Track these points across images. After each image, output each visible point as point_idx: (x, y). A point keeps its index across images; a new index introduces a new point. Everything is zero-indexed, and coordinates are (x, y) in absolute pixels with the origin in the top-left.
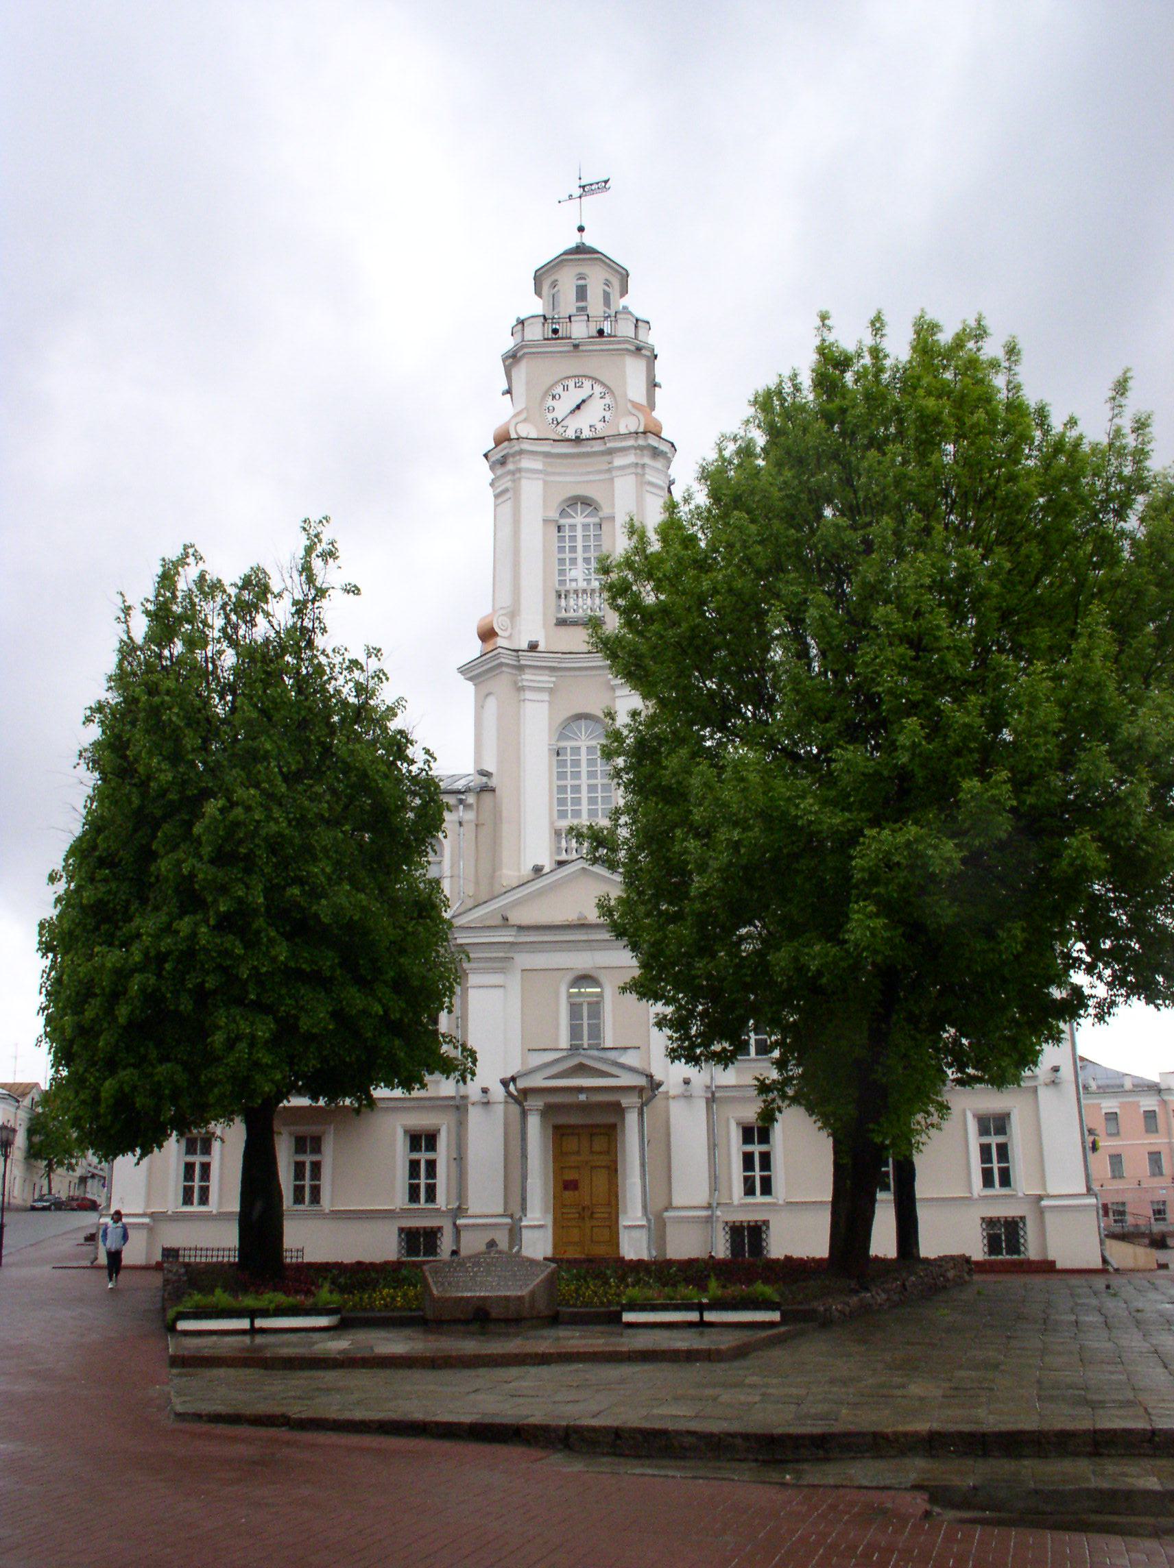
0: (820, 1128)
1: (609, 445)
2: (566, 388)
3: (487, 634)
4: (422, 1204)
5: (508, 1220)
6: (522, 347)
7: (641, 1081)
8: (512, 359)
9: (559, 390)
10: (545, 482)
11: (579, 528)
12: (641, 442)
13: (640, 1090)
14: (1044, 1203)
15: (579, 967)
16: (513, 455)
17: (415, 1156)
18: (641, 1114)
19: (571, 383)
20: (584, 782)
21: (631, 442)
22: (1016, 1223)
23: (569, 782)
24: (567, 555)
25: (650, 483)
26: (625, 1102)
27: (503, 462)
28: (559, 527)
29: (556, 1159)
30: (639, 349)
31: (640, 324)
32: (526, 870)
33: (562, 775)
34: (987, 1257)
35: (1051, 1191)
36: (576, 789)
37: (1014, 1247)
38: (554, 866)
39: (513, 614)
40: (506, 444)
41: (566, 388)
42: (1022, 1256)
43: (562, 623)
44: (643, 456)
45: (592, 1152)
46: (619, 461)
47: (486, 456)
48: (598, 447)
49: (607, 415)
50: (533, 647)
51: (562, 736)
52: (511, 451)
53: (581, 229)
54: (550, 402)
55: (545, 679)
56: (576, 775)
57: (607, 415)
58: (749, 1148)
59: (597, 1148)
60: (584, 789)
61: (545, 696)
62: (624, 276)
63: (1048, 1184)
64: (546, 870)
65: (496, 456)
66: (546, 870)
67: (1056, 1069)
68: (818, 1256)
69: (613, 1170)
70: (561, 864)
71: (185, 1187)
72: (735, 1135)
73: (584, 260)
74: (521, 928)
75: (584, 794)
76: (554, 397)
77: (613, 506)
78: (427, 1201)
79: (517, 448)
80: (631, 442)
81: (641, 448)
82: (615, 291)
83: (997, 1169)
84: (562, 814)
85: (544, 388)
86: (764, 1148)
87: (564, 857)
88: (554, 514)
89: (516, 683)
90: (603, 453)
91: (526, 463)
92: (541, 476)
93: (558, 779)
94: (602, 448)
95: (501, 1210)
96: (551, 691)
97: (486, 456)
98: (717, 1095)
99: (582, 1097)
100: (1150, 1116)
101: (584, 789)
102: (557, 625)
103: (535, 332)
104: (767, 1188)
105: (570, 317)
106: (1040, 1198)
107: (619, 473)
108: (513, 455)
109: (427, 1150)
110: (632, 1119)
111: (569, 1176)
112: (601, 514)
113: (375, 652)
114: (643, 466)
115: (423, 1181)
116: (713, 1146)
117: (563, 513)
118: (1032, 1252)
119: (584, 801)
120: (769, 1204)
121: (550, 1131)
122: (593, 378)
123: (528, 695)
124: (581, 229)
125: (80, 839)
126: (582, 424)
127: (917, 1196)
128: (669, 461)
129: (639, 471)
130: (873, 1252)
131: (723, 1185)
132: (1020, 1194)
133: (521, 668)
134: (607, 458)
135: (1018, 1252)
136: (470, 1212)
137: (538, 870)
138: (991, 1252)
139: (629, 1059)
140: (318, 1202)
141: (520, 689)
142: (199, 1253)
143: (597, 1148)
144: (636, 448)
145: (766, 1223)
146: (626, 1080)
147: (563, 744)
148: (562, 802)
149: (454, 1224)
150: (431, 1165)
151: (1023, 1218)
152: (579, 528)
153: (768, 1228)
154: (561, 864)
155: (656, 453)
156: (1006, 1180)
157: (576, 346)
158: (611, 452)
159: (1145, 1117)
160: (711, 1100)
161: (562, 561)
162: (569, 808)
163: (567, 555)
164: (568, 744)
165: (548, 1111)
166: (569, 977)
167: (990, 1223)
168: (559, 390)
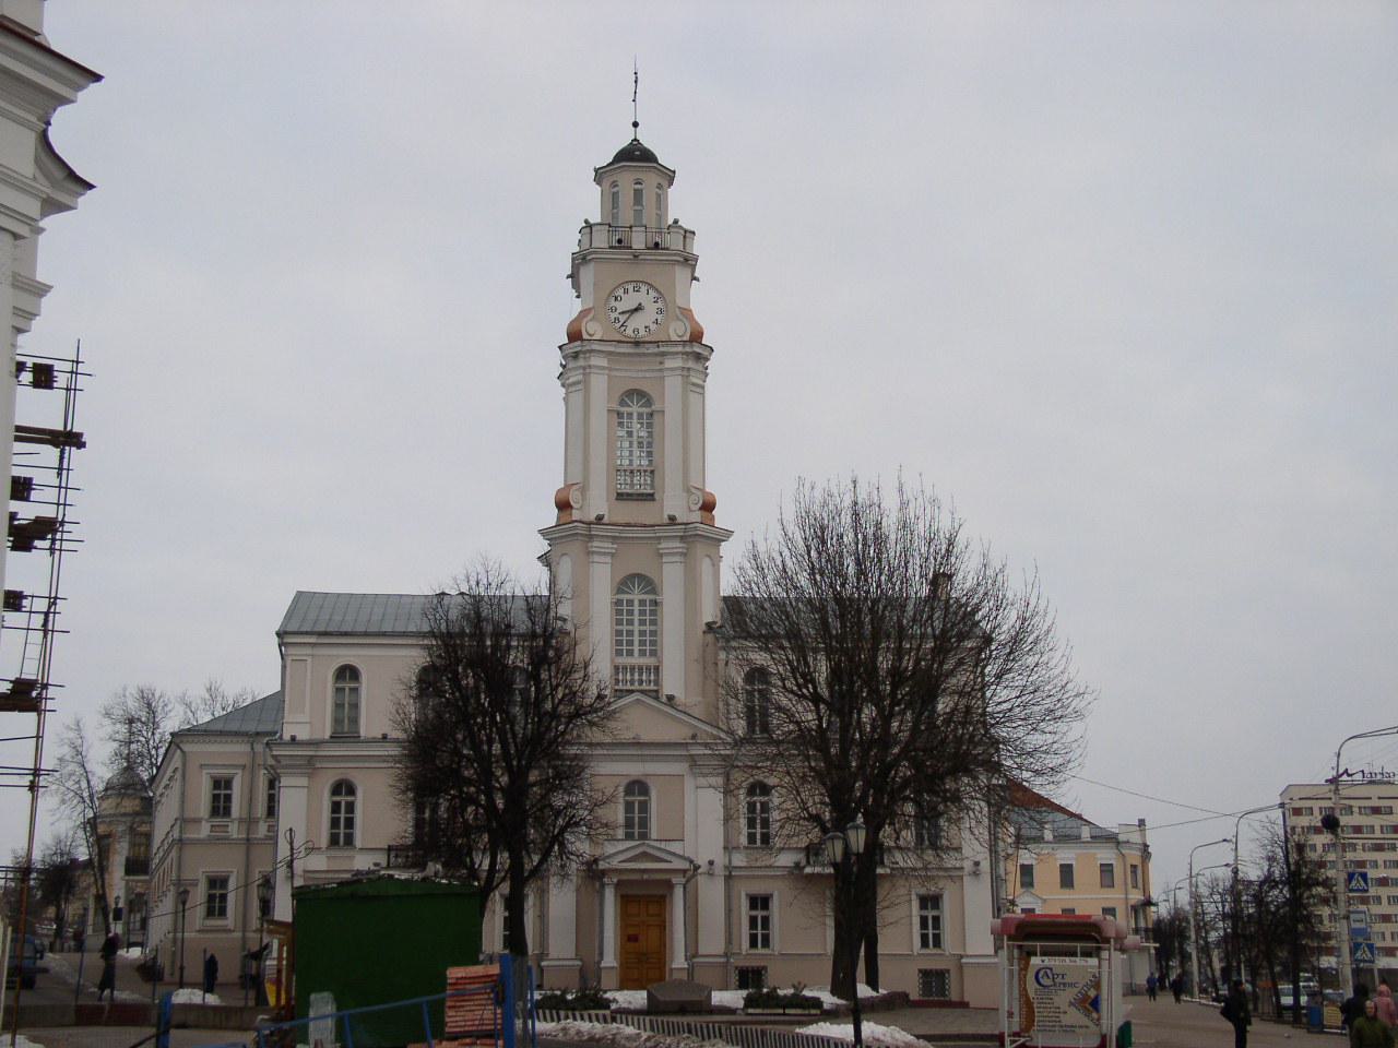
1: (662, 349)
3: (563, 505)
5: (579, 963)
6: (590, 253)
7: (686, 865)
8: (580, 260)
9: (620, 292)
10: (609, 376)
12: (688, 349)
13: (684, 871)
14: (964, 960)
16: (585, 353)
18: (684, 888)
19: (630, 287)
20: (636, 628)
21: (680, 349)
23: (625, 628)
25: (694, 384)
26: (674, 881)
27: (576, 356)
29: (622, 919)
31: (688, 234)
33: (619, 622)
34: (921, 998)
35: (969, 952)
37: (942, 990)
39: (584, 490)
40: (579, 343)
42: (947, 999)
43: (620, 496)
44: (687, 360)
45: (648, 915)
46: (670, 363)
47: (560, 347)
48: (653, 349)
49: (660, 305)
50: (600, 518)
52: (584, 349)
53: (635, 125)
55: (608, 546)
57: (659, 317)
58: (754, 913)
59: (651, 912)
61: (608, 559)
63: (967, 948)
65: (570, 350)
67: (977, 864)
69: (662, 926)
72: (745, 904)
75: (636, 638)
76: (616, 299)
77: (663, 402)
79: (588, 348)
80: (680, 349)
81: (687, 354)
83: (931, 933)
84: (619, 653)
85: (608, 292)
86: (765, 913)
88: (616, 406)
89: (587, 548)
90: (656, 355)
91: (596, 361)
92: (607, 372)
93: (656, 641)
94: (656, 350)
95: (573, 956)
96: (612, 555)
97: (560, 347)
98: (733, 874)
99: (646, 877)
100: (1107, 870)
103: (601, 240)
104: (766, 942)
105: (631, 227)
106: (962, 957)
107: (670, 373)
108: (585, 353)
110: (679, 892)
111: (631, 931)
112: (653, 407)
114: (689, 369)
116: (729, 911)
117: (622, 403)
118: (954, 996)
120: (766, 955)
121: (619, 898)
123: (596, 558)
124: (635, 125)
125: (1130, 1037)
126: (638, 324)
127: (879, 952)
129: (685, 373)
131: (735, 942)
132: (947, 953)
133: (591, 537)
134: (659, 359)
135: (944, 995)
138: (924, 994)
139: (675, 847)
140: (940, 947)
141: (589, 553)
143: (651, 912)
144: (683, 354)
145: (765, 968)
146: (678, 864)
147: (621, 596)
149: (539, 966)
151: (948, 971)
153: (766, 971)
155: (699, 358)
156: (937, 942)
157: (635, 256)
158: (663, 354)
159: (1101, 871)
160: (728, 878)
164: (625, 597)
165: (618, 885)
166: (625, 781)
167: (925, 974)
168: (620, 292)
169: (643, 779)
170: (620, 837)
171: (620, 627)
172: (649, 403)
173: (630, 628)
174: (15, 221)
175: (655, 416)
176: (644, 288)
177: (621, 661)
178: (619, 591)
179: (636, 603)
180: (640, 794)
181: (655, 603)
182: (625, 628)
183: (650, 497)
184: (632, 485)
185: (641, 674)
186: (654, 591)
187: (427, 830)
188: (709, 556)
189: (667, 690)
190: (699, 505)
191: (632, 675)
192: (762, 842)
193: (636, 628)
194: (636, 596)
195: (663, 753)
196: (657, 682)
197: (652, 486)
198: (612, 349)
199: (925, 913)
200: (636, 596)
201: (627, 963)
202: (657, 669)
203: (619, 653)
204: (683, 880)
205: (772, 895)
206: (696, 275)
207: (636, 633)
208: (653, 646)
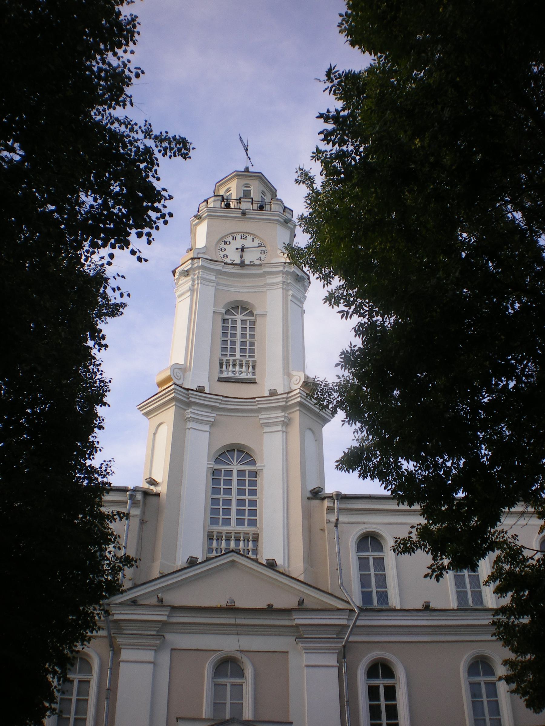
0: (344, 452)
2: (234, 239)
10: (216, 289)
11: (239, 322)
15: (226, 649)
20: (234, 496)
23: (222, 496)
32: (181, 561)
33: (215, 491)
36: (228, 502)
41: (234, 239)
50: (201, 390)
51: (217, 461)
54: (223, 246)
56: (228, 491)
61: (207, 428)
64: (199, 561)
70: (208, 559)
73: (321, 653)
74: (174, 609)
93: (213, 493)
96: (212, 425)
102: (218, 381)
113: (171, 215)
117: (228, 312)
123: (190, 425)
147: (227, 317)
148: (215, 511)
152: (239, 322)
164: (223, 467)
166: (213, 658)
169: (238, 655)
174: (317, 655)
177: (216, 528)
179: (235, 473)
182: (222, 496)
183: (253, 382)
186: (253, 462)
189: (265, 555)
190: (301, 383)
194: (235, 467)
195: (239, 621)
198: (220, 268)
199: (374, 682)
200: (235, 467)
202: (256, 540)
203: (214, 521)
206: (295, 605)
208: (250, 512)
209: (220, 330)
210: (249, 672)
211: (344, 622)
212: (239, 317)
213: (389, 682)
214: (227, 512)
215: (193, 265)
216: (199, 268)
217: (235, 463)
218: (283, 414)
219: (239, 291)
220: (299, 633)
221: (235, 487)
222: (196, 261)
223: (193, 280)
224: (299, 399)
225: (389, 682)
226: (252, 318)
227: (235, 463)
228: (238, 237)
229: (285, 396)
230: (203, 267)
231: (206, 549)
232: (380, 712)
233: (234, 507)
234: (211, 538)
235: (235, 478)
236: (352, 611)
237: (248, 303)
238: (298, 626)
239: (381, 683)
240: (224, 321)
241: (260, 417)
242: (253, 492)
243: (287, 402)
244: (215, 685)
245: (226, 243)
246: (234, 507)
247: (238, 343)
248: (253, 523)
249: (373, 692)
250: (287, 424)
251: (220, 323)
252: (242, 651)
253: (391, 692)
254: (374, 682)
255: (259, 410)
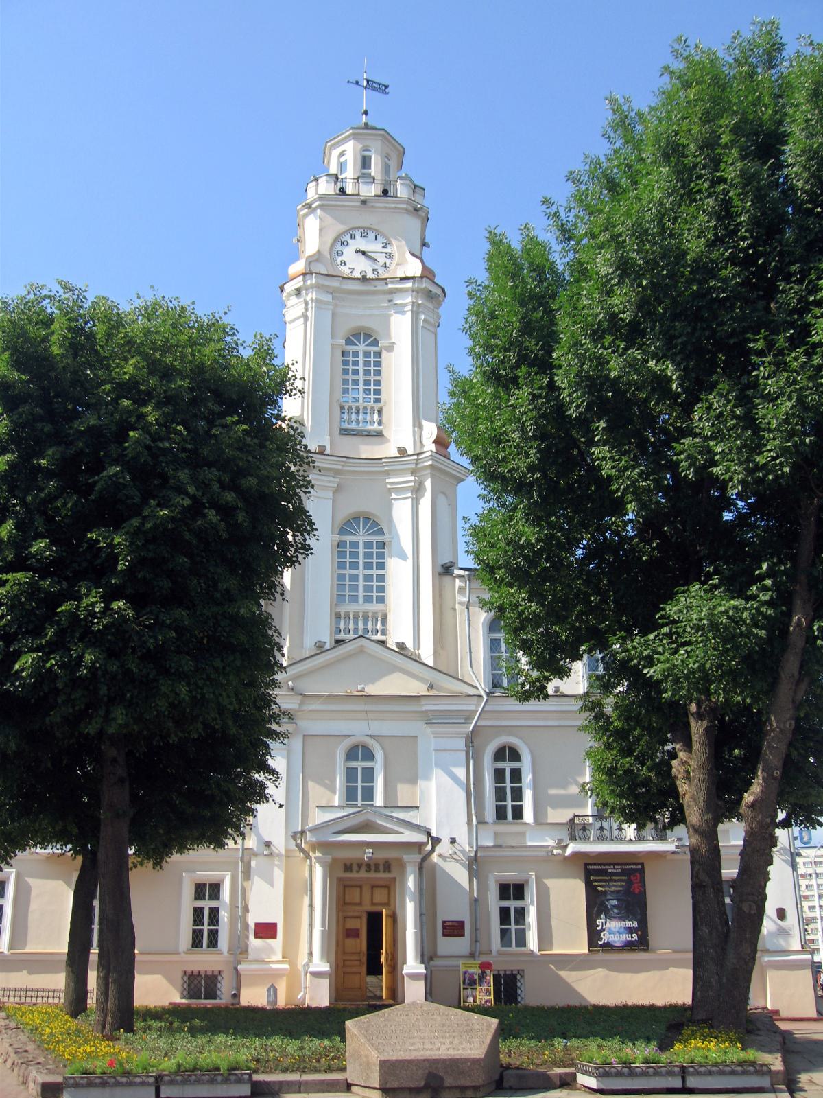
1: (390, 286)
4: (514, 948)
7: (421, 838)
11: (361, 355)
13: (420, 846)
17: (200, 904)
20: (361, 572)
22: (515, 976)
24: (351, 377)
26: (406, 858)
28: (343, 352)
30: (416, 210)
32: (309, 644)
33: (341, 565)
36: (354, 577)
38: (333, 643)
48: (380, 286)
56: (354, 566)
60: (361, 578)
62: (402, 154)
64: (327, 646)
66: (327, 646)
68: (680, 1002)
71: (194, 931)
76: (342, 243)
78: (517, 946)
82: (393, 164)
87: (342, 636)
101: (361, 578)
109: (211, 898)
115: (206, 928)
117: (349, 342)
119: (361, 588)
122: (376, 230)
128: (439, 305)
130: (328, 1004)
134: (389, 297)
136: (251, 957)
137: (320, 647)
142: (29, 993)
148: (341, 587)
150: (214, 912)
154: (339, 642)
157: (364, 202)
158: (392, 292)
161: (345, 381)
162: (347, 593)
163: (351, 377)
164: (349, 538)
166: (346, 744)
168: (347, 238)
169: (369, 741)
170: (337, 804)
171: (346, 377)
172: (375, 343)
173: (355, 377)
175: (384, 354)
176: (372, 235)
178: (342, 531)
179: (361, 545)
180: (364, 759)
181: (382, 545)
184: (357, 422)
185: (366, 623)
187: (43, 495)
188: (444, 493)
191: (356, 623)
192: (514, 818)
193: (361, 572)
194: (361, 538)
196: (384, 632)
197: (380, 423)
200: (361, 538)
201: (344, 966)
202: (385, 619)
204: (418, 858)
205: (527, 881)
207: (361, 566)
209: (339, 367)
210: (379, 755)
211: (473, 708)
212: (361, 348)
213: (515, 765)
214: (355, 588)
215: (305, 281)
216: (312, 287)
217: (361, 533)
218: (413, 478)
219: (358, 314)
220: (431, 719)
221: (361, 560)
222: (308, 277)
223: (306, 303)
224: (430, 462)
225: (515, 765)
226: (380, 538)
227: (361, 533)
228: (358, 234)
229: (415, 457)
230: (318, 287)
231: (334, 629)
232: (505, 793)
233: (361, 583)
234: (338, 616)
235: (361, 550)
236: (480, 696)
237: (372, 330)
238: (427, 711)
239: (508, 766)
240: (344, 353)
241: (388, 481)
242: (378, 373)
243: (417, 464)
244: (345, 887)
245: (342, 243)
246: (361, 583)
247: (361, 372)
248: (382, 600)
249: (499, 775)
250: (418, 490)
251: (339, 358)
252: (372, 737)
253: (516, 775)
254: (500, 765)
255: (387, 474)
